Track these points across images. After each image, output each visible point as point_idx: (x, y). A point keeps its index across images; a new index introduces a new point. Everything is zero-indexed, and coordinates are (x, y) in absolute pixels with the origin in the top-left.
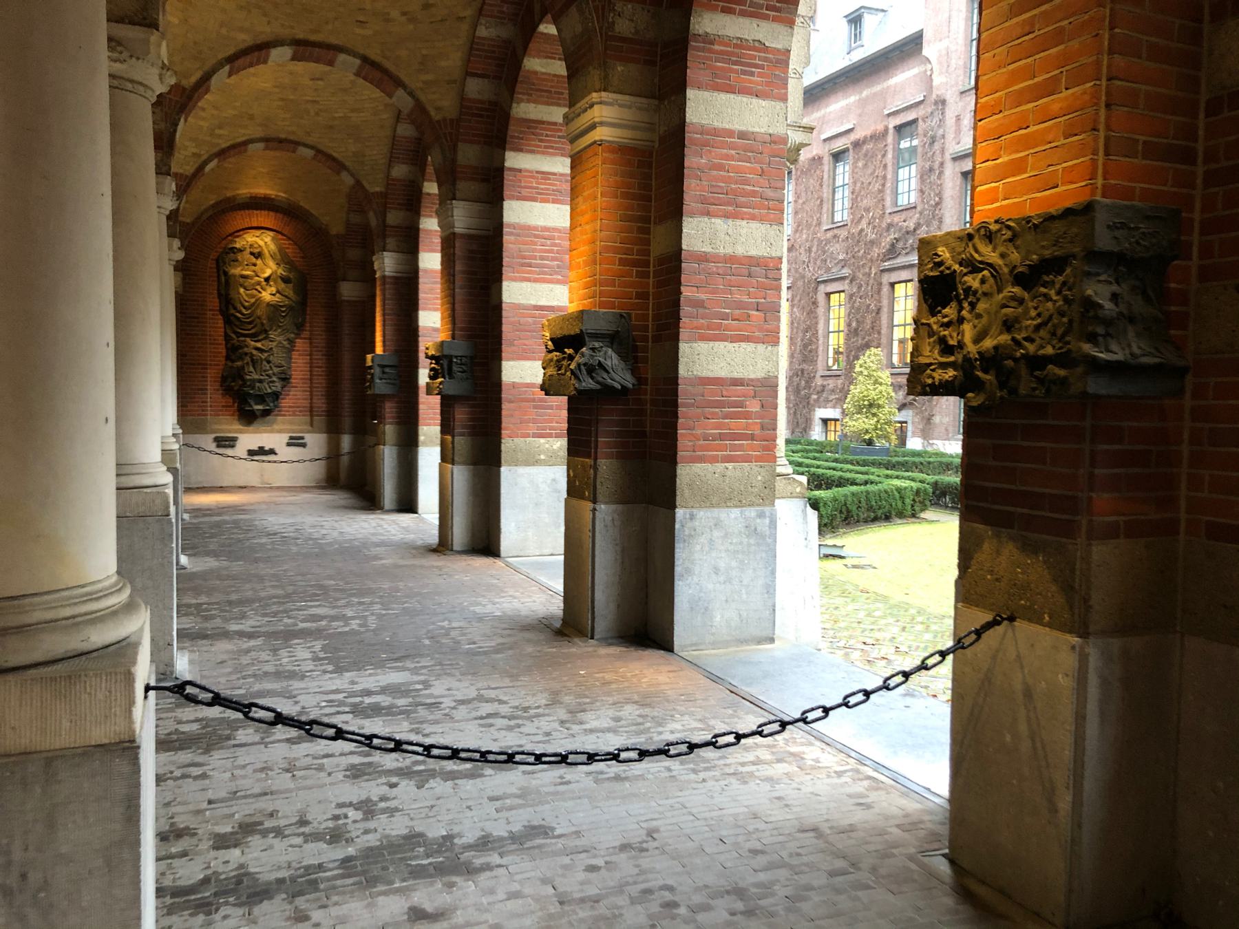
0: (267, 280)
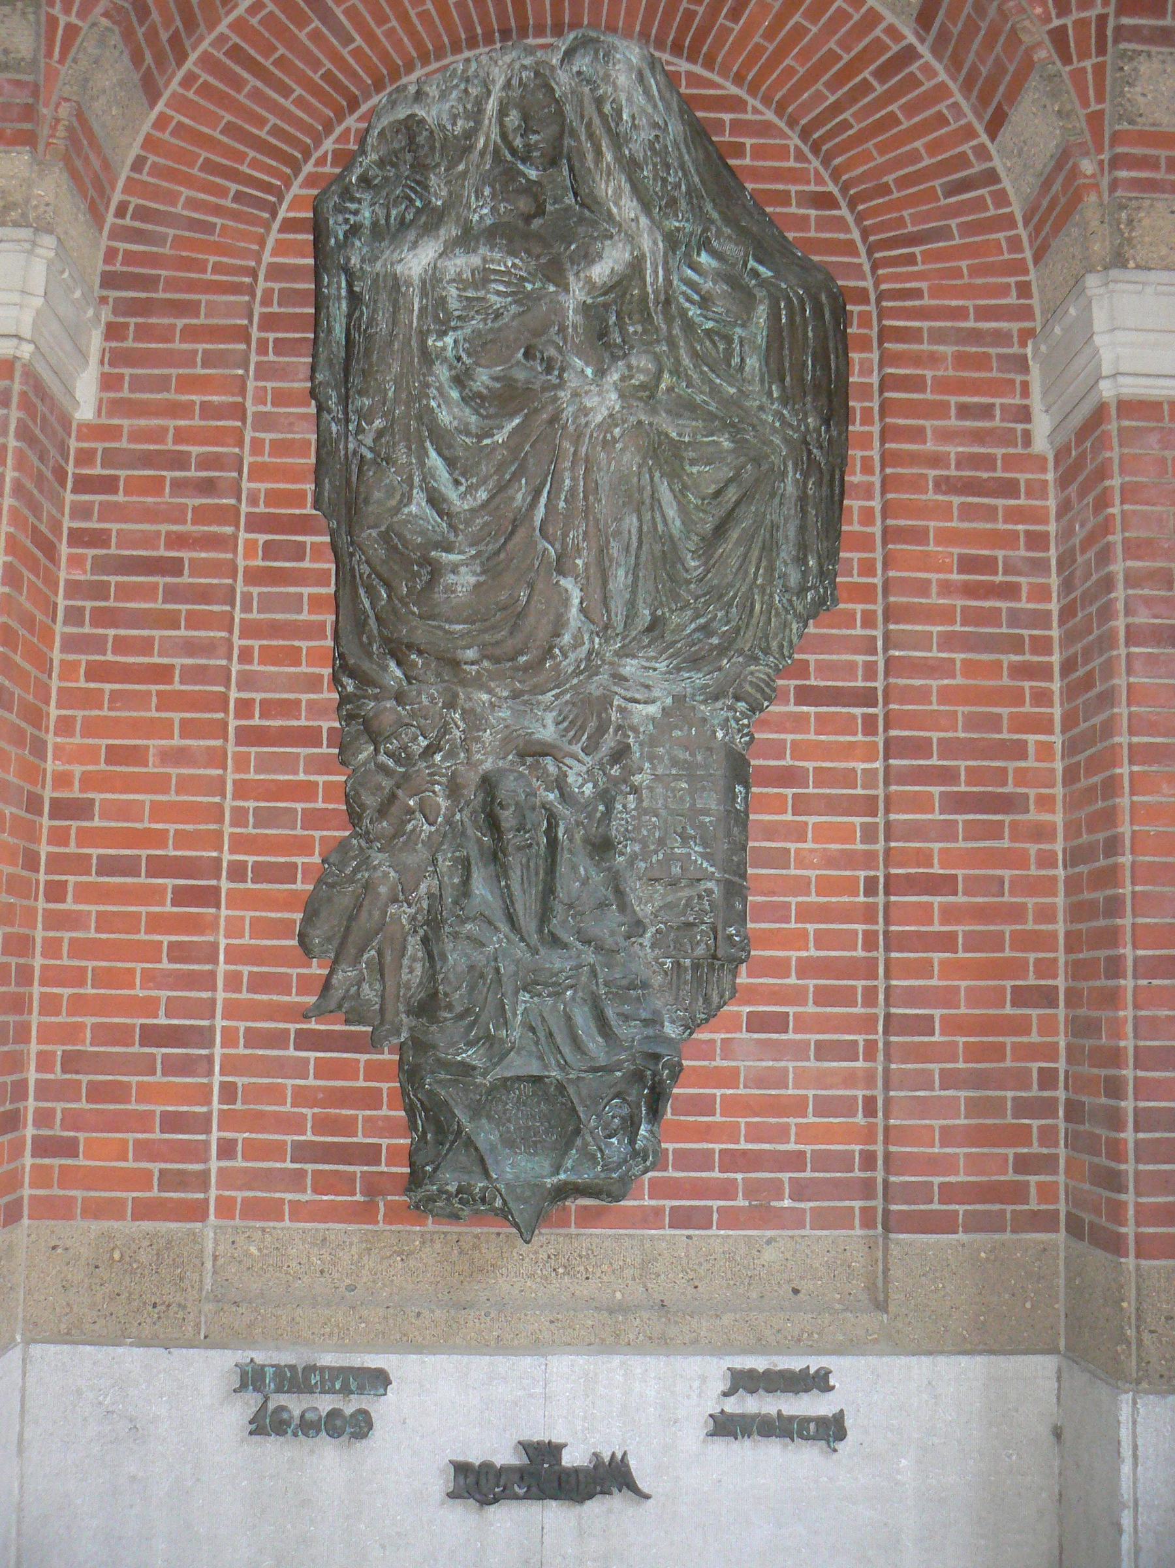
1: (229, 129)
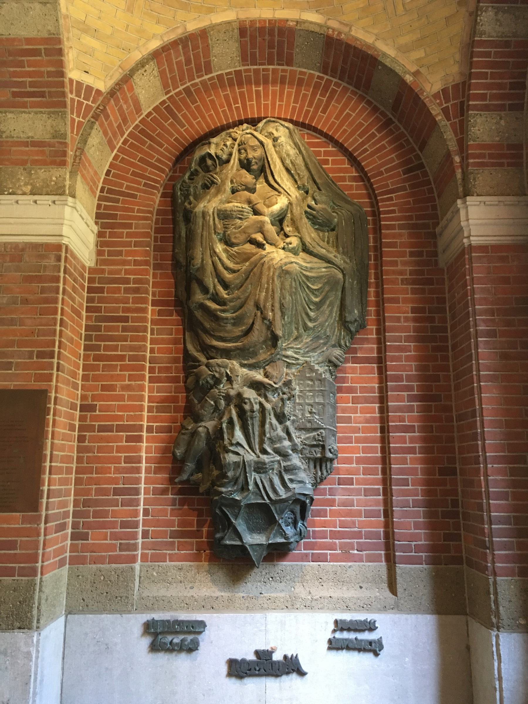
0: (279, 220)
1: (141, 160)
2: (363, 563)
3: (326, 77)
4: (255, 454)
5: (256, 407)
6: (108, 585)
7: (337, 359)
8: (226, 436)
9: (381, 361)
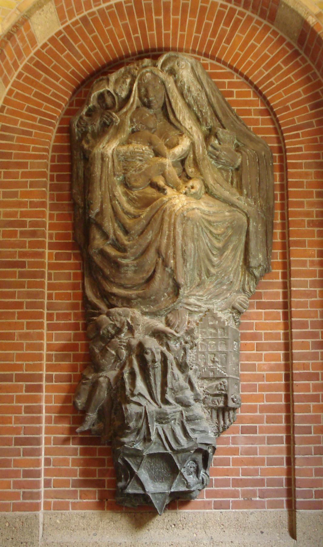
1: (37, 95)
2: (264, 510)
3: (229, 5)
4: (157, 405)
5: (158, 357)
6: (13, 532)
7: (241, 305)
8: (128, 387)
9: (286, 305)
